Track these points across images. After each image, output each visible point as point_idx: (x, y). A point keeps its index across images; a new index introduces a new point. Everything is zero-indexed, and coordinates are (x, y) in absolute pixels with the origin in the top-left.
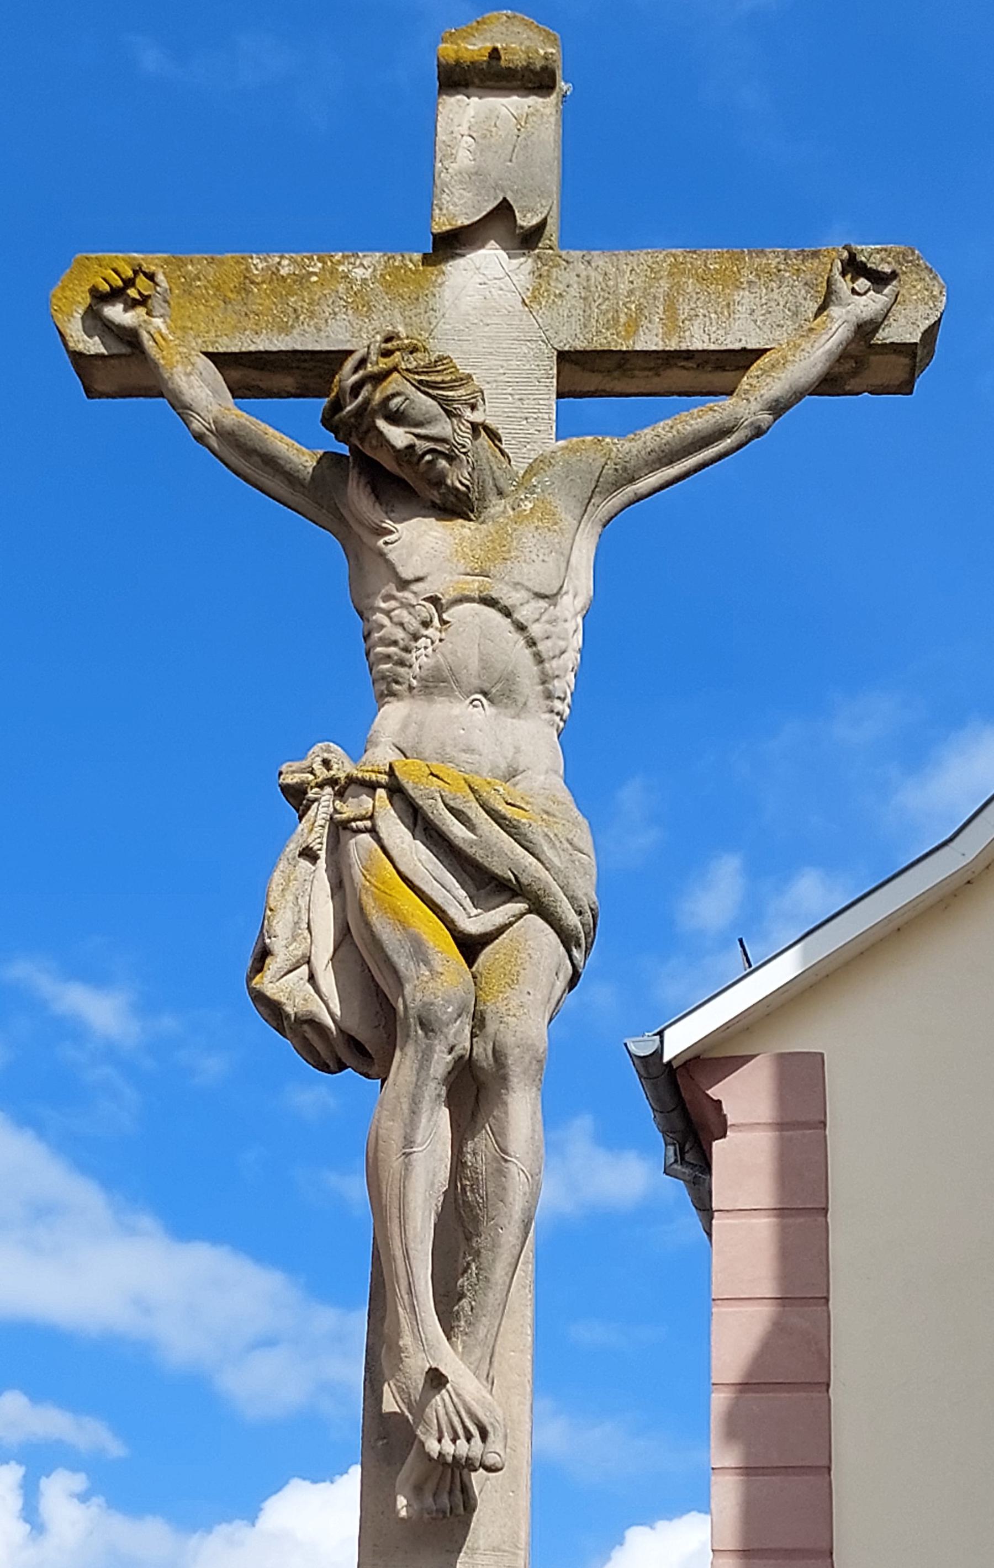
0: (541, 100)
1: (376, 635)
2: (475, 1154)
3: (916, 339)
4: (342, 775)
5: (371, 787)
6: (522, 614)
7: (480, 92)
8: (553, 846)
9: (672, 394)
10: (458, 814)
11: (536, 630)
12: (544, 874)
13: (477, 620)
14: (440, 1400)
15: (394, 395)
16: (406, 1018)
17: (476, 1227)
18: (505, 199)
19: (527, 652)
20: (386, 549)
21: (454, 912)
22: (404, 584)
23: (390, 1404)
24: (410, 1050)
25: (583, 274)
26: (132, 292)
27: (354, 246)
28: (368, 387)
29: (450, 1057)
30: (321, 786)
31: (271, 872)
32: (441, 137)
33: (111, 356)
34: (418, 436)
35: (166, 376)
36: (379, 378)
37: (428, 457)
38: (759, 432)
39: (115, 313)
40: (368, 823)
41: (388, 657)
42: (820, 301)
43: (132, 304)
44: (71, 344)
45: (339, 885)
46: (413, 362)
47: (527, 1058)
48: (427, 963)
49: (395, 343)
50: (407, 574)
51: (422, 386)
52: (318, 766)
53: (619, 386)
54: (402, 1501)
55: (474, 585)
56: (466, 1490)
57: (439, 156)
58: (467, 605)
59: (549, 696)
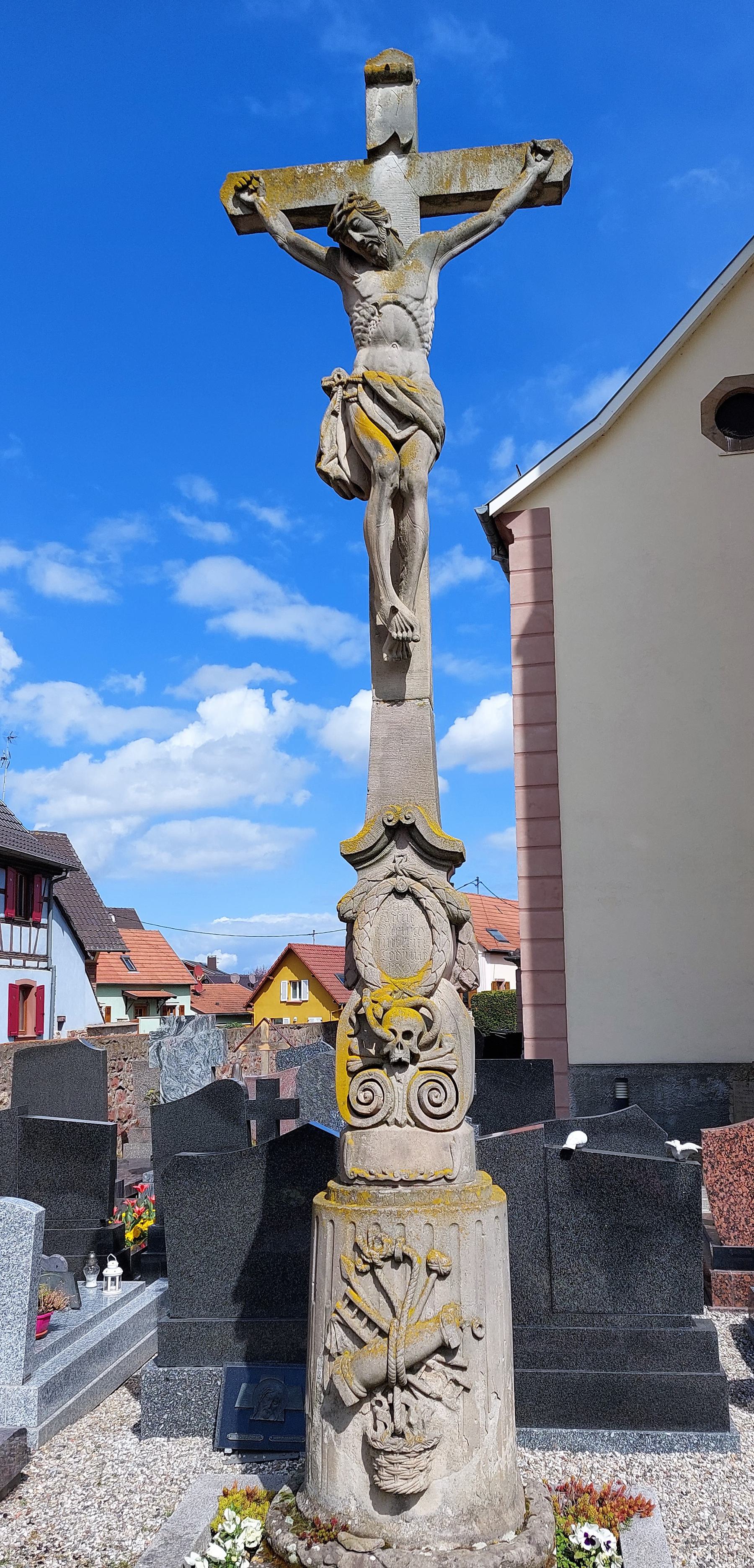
0: (407, 87)
1: (355, 322)
2: (403, 525)
3: (561, 179)
4: (345, 381)
5: (356, 384)
6: (410, 307)
7: (382, 85)
8: (427, 402)
9: (466, 212)
10: (389, 391)
11: (416, 314)
12: (423, 413)
13: (393, 311)
14: (396, 618)
15: (355, 219)
16: (375, 474)
17: (406, 553)
18: (395, 132)
19: (413, 323)
20: (356, 285)
21: (390, 431)
22: (364, 299)
23: (379, 622)
24: (377, 486)
25: (428, 162)
26: (251, 187)
27: (337, 159)
28: (344, 216)
29: (391, 488)
30: (337, 386)
31: (321, 422)
32: (368, 107)
33: (245, 215)
34: (365, 236)
35: (267, 221)
36: (348, 212)
37: (370, 245)
38: (500, 224)
39: (245, 196)
40: (356, 398)
41: (360, 330)
42: (523, 166)
43: (251, 192)
44: (229, 212)
45: (347, 425)
46: (361, 204)
47: (421, 486)
48: (381, 452)
49: (354, 196)
50: (364, 294)
51: (366, 214)
52: (336, 378)
53: (445, 211)
54: (385, 655)
55: (390, 297)
56: (408, 650)
57: (367, 115)
58: (388, 306)
59: (422, 341)
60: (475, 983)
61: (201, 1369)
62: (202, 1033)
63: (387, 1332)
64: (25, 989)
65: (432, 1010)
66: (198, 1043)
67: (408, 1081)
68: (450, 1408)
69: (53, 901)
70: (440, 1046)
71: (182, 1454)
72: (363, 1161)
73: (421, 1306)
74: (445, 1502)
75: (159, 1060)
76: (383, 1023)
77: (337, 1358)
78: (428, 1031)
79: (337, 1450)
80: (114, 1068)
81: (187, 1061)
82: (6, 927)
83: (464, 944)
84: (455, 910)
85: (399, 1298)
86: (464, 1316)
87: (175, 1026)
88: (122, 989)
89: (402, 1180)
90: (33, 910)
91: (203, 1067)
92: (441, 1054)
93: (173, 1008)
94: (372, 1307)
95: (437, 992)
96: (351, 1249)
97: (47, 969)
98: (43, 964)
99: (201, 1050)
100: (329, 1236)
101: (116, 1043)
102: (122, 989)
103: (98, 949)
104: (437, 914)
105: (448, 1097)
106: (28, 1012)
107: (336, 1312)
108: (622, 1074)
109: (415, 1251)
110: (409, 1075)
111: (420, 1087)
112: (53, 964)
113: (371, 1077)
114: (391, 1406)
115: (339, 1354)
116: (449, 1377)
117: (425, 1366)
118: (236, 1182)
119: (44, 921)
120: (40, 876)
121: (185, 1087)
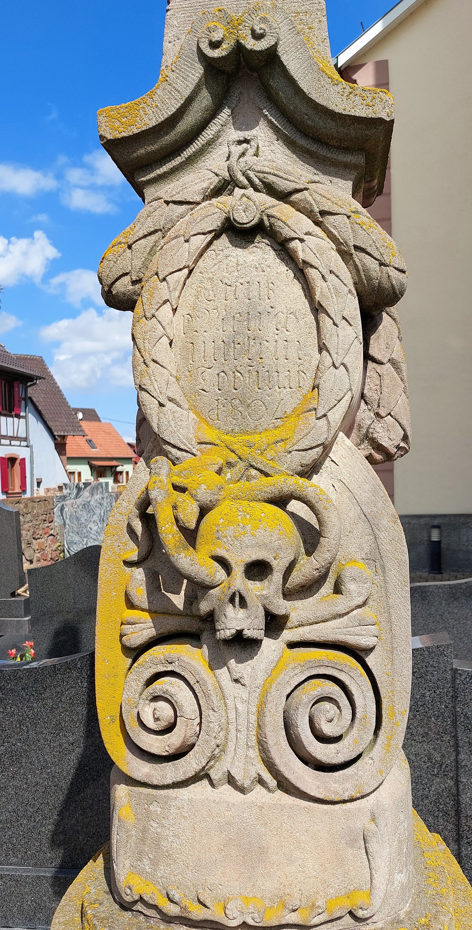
60: (402, 444)
62: (98, 497)
64: (12, 460)
65: (319, 506)
66: (94, 505)
67: (260, 681)
69: (28, 400)
70: (337, 590)
72: (154, 863)
75: (63, 519)
76: (199, 540)
78: (309, 553)
80: (45, 520)
81: (86, 520)
82: (3, 419)
83: (382, 363)
84: (373, 265)
87: (75, 491)
88: (88, 460)
89: (244, 923)
90: (14, 406)
91: (99, 525)
92: (341, 609)
93: (121, 473)
95: (327, 462)
97: (27, 446)
98: (24, 443)
99: (98, 511)
101: (46, 502)
102: (88, 460)
103: (66, 434)
104: (331, 278)
105: (358, 715)
106: (15, 475)
108: (436, 522)
110: (263, 666)
111: (288, 696)
112: (31, 444)
113: (170, 668)
118: (50, 702)
119: (22, 414)
120: (18, 382)
121: (85, 541)
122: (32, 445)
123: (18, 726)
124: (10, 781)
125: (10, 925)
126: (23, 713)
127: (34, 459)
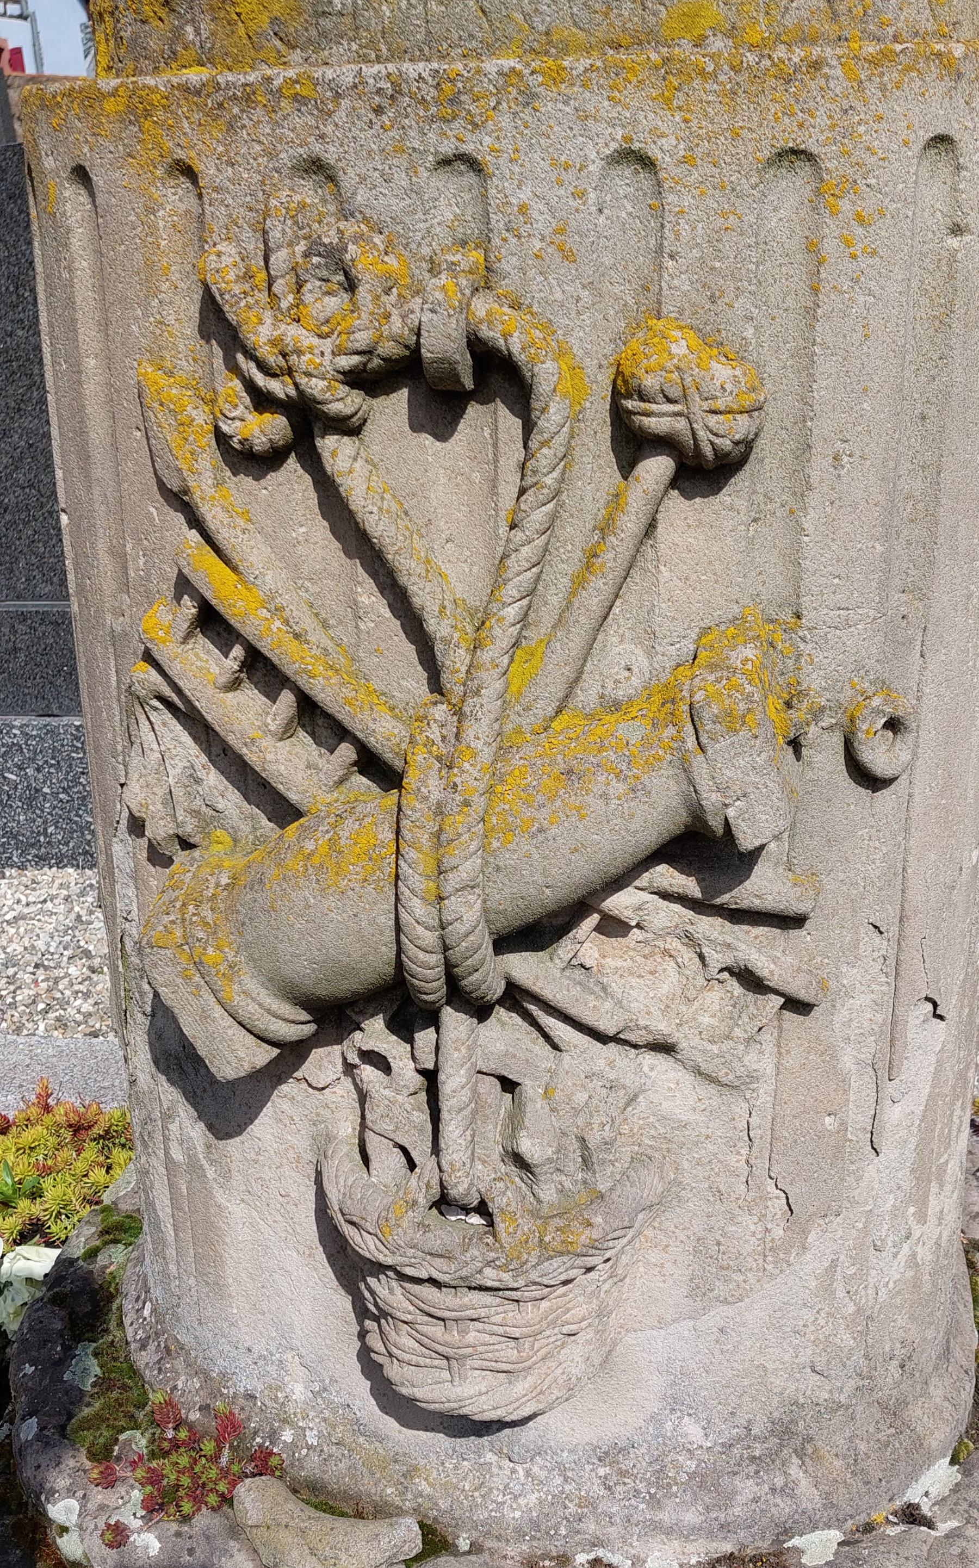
61: (54, 721)
63: (398, 764)
68: (713, 1080)
71: (26, 911)
73: (576, 640)
74: (675, 1403)
77: (181, 857)
79: (220, 1197)
85: (460, 590)
86: (814, 681)
94: (316, 636)
96: (191, 329)
97: (22, 17)
100: (84, 265)
107: (149, 657)
109: (548, 327)
112: (31, 9)
114: (431, 1077)
115: (186, 845)
116: (716, 959)
117: (594, 919)
122: (34, 13)
123: (11, 289)
124: (12, 418)
125: (55, 712)
126: (20, 256)
127: (44, 50)
